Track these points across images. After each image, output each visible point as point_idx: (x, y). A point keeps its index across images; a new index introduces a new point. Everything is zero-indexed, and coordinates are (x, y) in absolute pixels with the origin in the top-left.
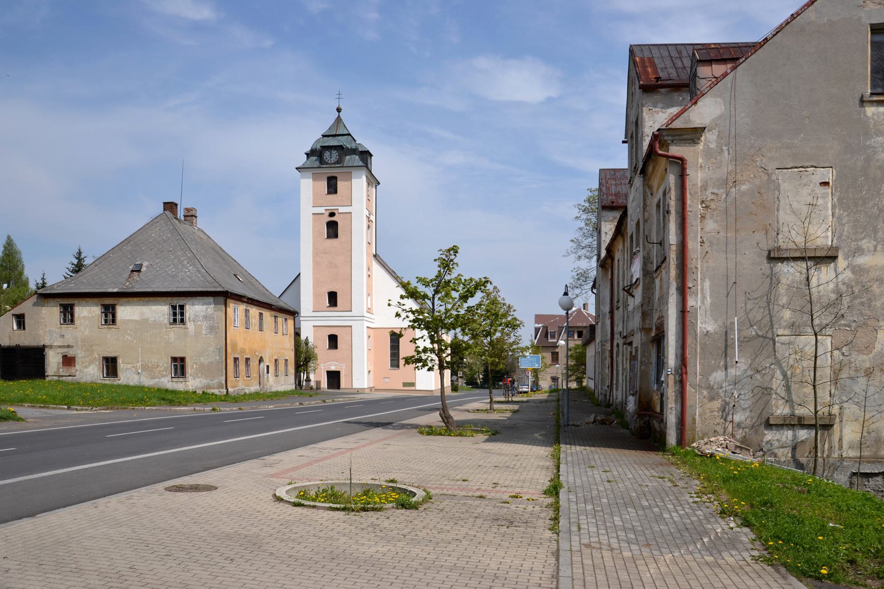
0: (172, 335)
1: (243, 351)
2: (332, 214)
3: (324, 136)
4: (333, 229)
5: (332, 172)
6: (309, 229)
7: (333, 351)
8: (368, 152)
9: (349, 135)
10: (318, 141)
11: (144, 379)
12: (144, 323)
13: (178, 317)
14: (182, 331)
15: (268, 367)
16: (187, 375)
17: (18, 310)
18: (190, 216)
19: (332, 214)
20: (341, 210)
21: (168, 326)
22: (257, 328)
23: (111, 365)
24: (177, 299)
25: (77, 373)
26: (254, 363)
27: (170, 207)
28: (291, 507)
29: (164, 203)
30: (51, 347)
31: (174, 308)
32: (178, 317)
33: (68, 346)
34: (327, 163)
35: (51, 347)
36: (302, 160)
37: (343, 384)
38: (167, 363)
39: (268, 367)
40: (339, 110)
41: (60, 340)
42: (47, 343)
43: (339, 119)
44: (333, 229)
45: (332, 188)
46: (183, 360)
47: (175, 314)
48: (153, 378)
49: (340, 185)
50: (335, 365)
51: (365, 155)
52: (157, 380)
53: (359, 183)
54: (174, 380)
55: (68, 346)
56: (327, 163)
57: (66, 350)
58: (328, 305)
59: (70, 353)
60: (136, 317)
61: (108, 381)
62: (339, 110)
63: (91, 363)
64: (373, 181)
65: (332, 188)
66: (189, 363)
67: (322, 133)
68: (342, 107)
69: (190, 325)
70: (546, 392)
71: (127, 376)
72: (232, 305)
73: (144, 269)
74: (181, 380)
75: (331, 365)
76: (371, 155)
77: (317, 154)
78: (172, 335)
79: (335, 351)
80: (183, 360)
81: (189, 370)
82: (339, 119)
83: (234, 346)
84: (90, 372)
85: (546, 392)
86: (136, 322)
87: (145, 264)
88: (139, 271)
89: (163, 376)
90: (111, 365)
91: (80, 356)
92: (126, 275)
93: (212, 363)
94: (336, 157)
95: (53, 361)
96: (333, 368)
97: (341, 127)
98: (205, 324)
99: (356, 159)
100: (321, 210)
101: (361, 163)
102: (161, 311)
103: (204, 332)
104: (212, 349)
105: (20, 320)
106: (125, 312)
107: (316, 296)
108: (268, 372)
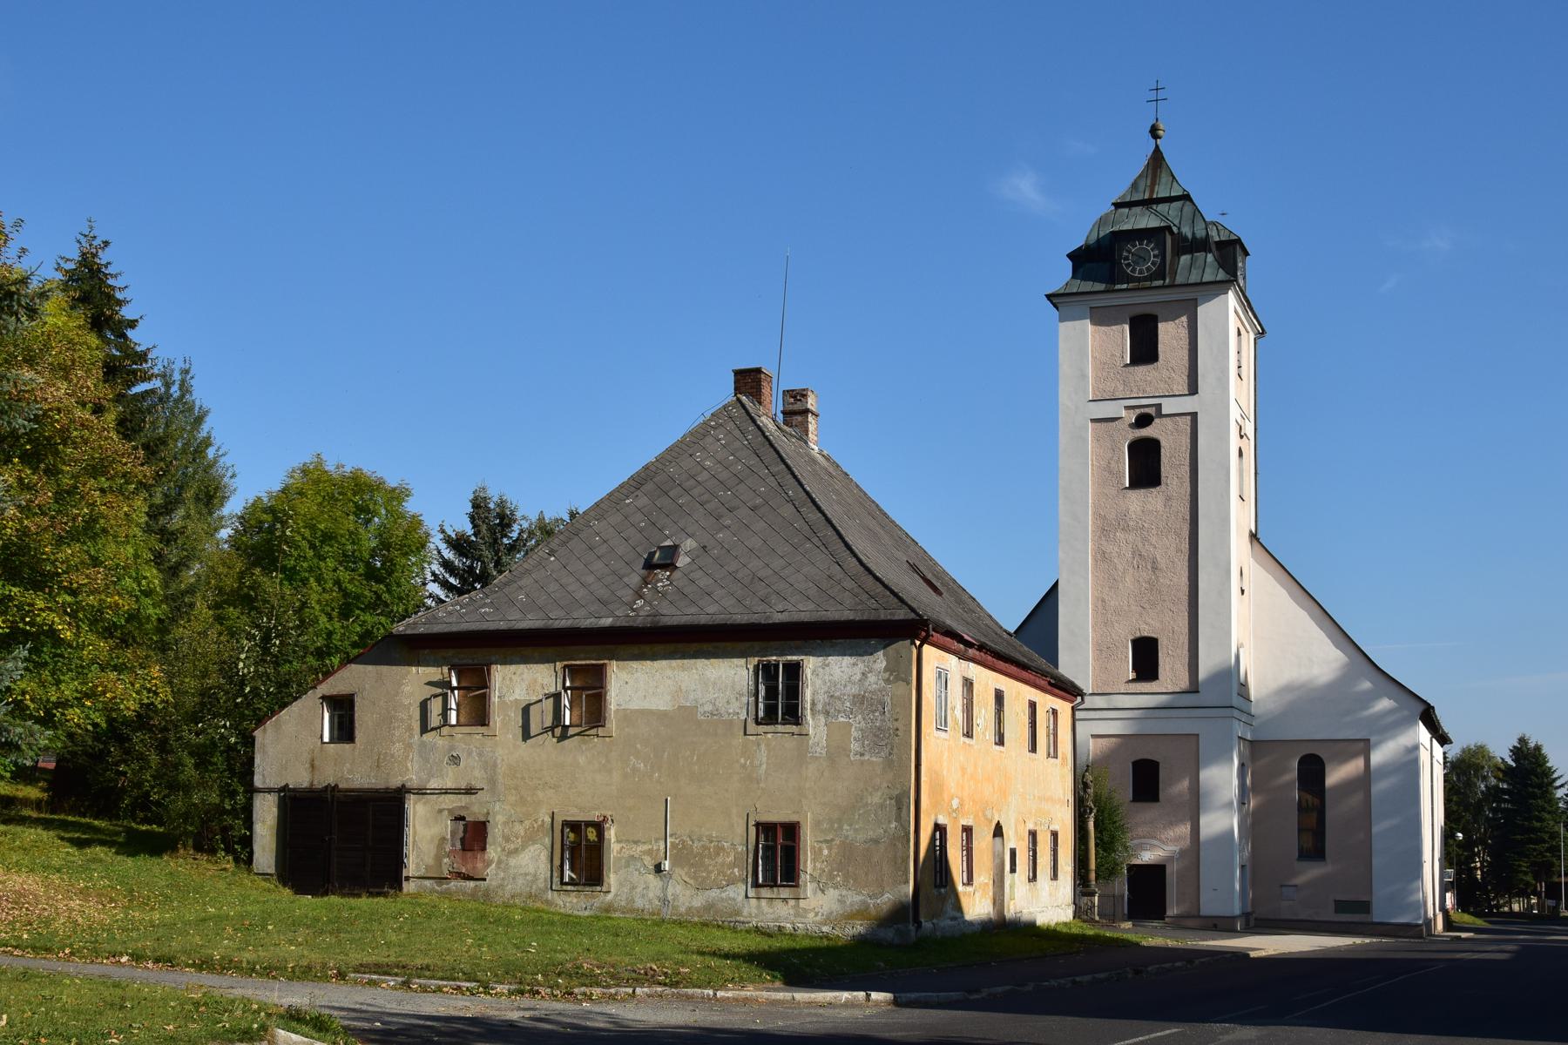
0: (762, 756)
3: (1117, 205)
4: (1145, 465)
5: (1142, 300)
6: (1087, 462)
8: (1238, 241)
9: (1186, 197)
10: (1102, 221)
11: (679, 889)
12: (683, 720)
13: (780, 703)
14: (790, 743)
15: (1013, 853)
16: (804, 878)
17: (336, 685)
18: (796, 412)
19: (1144, 421)
21: (752, 727)
22: (990, 736)
23: (583, 853)
24: (772, 647)
25: (491, 870)
26: (983, 842)
27: (749, 381)
29: (738, 373)
30: (421, 792)
31: (768, 672)
32: (780, 703)
33: (470, 791)
35: (421, 792)
36: (1061, 275)
38: (736, 839)
39: (1013, 853)
40: (1154, 132)
41: (451, 771)
42: (413, 778)
43: (1157, 159)
45: (1145, 351)
46: (792, 830)
47: (771, 693)
48: (701, 887)
51: (1230, 252)
52: (714, 893)
54: (765, 892)
55: (470, 791)
56: (1129, 279)
57: (464, 800)
58: (1131, 675)
59: (475, 808)
60: (661, 703)
61: (573, 903)
62: (1154, 132)
63: (530, 839)
65: (1145, 351)
66: (809, 839)
69: (814, 725)
71: (628, 882)
73: (682, 561)
74: (785, 893)
78: (762, 756)
80: (792, 830)
81: (809, 864)
82: (1157, 159)
83: (938, 788)
84: (522, 864)
86: (662, 716)
87: (689, 544)
88: (670, 566)
89: (731, 882)
90: (583, 853)
91: (500, 818)
92: (635, 580)
93: (876, 841)
94: (1142, 269)
95: (425, 833)
97: (1165, 178)
98: (857, 723)
102: (727, 680)
103: (855, 746)
104: (876, 799)
105: (343, 710)
106: (634, 685)
107: (1104, 650)
108: (1013, 870)
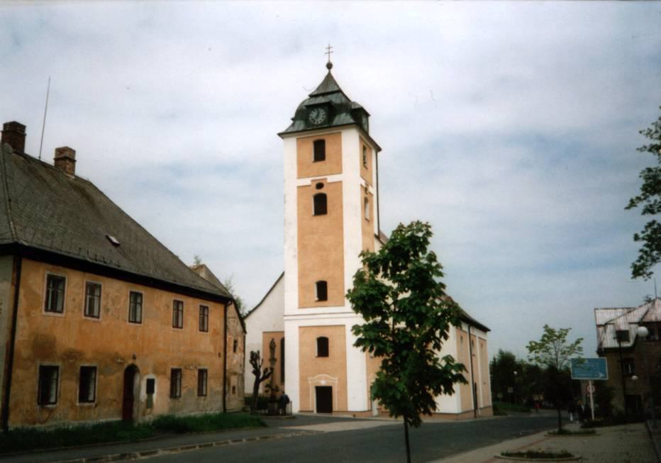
1: (71, 355)
2: (320, 186)
4: (321, 205)
7: (322, 360)
20: (331, 179)
28: (654, 286)
34: (313, 125)
37: (336, 405)
40: (329, 66)
44: (321, 205)
49: (329, 149)
50: (326, 379)
53: (350, 142)
62: (329, 66)
64: (370, 146)
67: (310, 93)
68: (332, 61)
70: (366, 285)
72: (27, 266)
75: (320, 379)
76: (367, 115)
77: (303, 113)
79: (325, 359)
82: (329, 79)
85: (366, 285)
96: (323, 383)
99: (344, 118)
100: (307, 181)
101: (352, 121)
107: (303, 288)
